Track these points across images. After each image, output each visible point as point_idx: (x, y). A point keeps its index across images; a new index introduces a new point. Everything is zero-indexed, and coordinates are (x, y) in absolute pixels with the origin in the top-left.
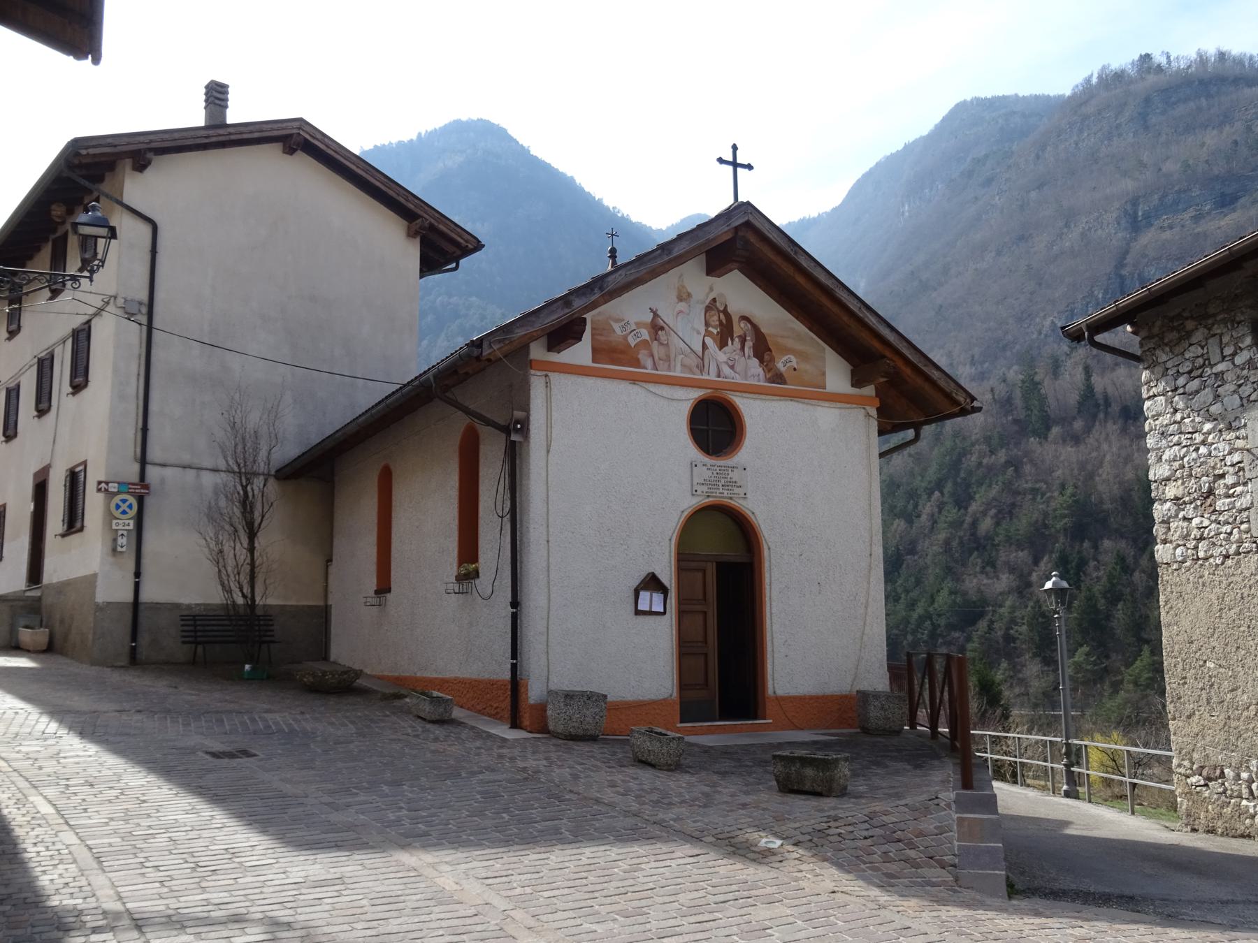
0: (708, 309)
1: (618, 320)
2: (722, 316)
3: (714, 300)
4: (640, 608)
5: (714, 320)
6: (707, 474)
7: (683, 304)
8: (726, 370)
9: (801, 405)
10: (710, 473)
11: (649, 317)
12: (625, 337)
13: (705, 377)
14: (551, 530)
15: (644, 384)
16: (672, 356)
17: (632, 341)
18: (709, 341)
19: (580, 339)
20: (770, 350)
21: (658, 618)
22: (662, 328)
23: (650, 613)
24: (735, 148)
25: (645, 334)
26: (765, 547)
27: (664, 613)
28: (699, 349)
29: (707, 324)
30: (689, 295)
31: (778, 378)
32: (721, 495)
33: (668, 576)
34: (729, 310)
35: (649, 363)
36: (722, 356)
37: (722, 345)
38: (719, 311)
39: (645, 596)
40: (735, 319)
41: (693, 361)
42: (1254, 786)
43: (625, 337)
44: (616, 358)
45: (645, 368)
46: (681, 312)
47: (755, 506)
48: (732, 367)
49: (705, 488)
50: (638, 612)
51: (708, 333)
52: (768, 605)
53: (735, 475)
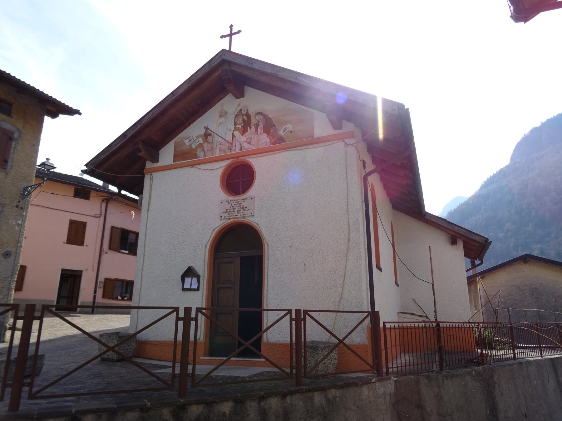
0: (236, 116)
1: (187, 139)
2: (245, 118)
3: (241, 110)
4: (185, 287)
5: (240, 120)
6: (228, 206)
7: (223, 118)
8: (246, 146)
9: (294, 152)
10: (230, 205)
11: (203, 131)
12: (190, 146)
13: (233, 152)
14: (146, 249)
15: (198, 166)
16: (215, 147)
17: (194, 146)
18: (236, 133)
19: (335, 129)
20: (274, 126)
21: (196, 292)
22: (210, 135)
23: (190, 290)
24: (222, 37)
25: (201, 140)
26: (266, 244)
27: (198, 289)
28: (229, 138)
29: (235, 124)
30: (226, 113)
31: (281, 140)
32: (237, 217)
33: (202, 266)
34: (249, 112)
35: (202, 154)
36: (243, 139)
37: (244, 131)
38: (243, 115)
39: (188, 280)
40: (253, 116)
41: (227, 145)
42: (133, 415)
43: (190, 146)
44: (185, 157)
45: (199, 157)
46: (221, 123)
47: (259, 221)
48: (249, 143)
49: (226, 215)
50: (184, 289)
51: (236, 129)
52: (266, 281)
53: (245, 204)
